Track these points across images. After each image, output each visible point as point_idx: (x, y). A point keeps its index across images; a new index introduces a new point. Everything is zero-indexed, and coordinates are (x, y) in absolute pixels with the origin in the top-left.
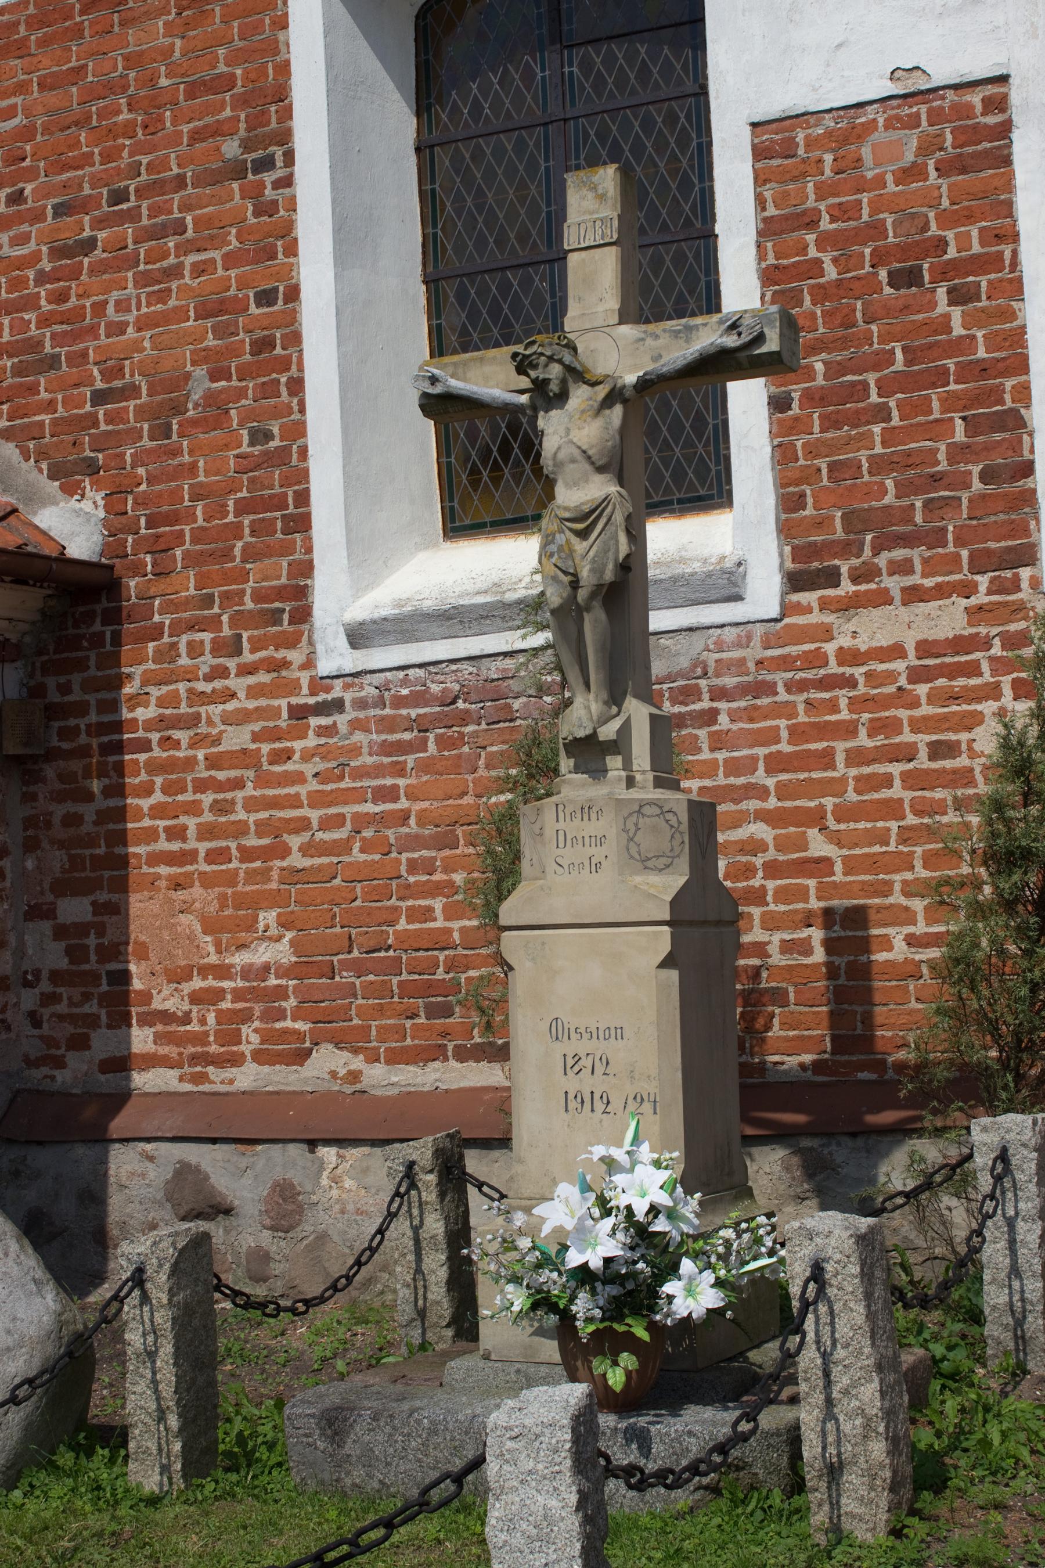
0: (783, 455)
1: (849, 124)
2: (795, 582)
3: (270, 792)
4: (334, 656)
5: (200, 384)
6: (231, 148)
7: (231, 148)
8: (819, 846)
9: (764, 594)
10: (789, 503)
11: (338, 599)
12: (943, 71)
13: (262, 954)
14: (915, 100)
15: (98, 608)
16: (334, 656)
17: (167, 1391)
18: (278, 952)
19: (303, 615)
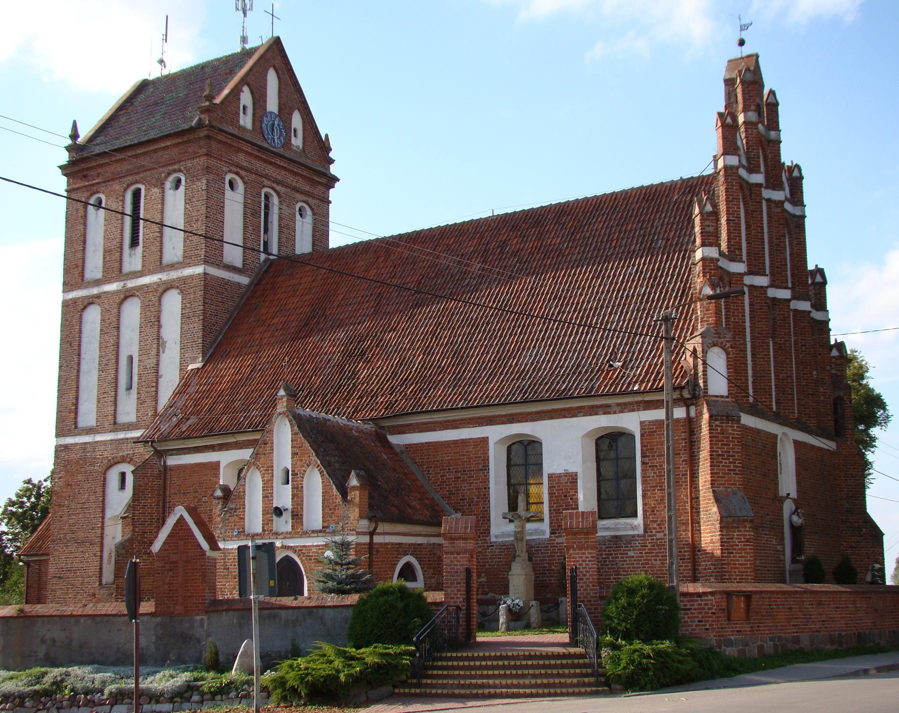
0: (550, 517)
1: (559, 476)
2: (551, 533)
3: (569, 589)
4: (493, 539)
5: (475, 499)
6: (481, 467)
7: (481, 467)
8: (553, 567)
9: (547, 535)
10: (551, 523)
11: (494, 531)
12: (570, 471)
13: (482, 580)
14: (567, 474)
15: (190, 150)
16: (493, 539)
17: (461, 705)
18: (484, 579)
19: (489, 533)
